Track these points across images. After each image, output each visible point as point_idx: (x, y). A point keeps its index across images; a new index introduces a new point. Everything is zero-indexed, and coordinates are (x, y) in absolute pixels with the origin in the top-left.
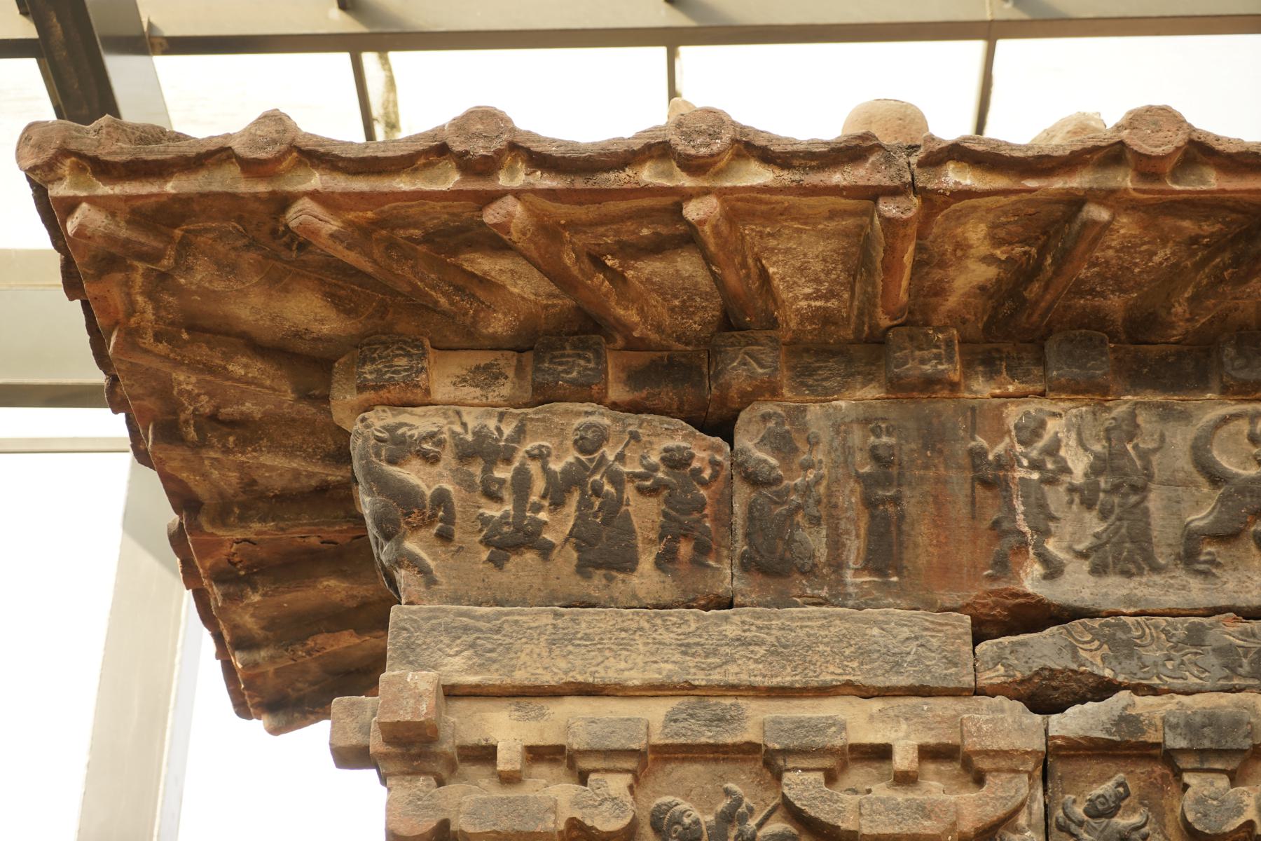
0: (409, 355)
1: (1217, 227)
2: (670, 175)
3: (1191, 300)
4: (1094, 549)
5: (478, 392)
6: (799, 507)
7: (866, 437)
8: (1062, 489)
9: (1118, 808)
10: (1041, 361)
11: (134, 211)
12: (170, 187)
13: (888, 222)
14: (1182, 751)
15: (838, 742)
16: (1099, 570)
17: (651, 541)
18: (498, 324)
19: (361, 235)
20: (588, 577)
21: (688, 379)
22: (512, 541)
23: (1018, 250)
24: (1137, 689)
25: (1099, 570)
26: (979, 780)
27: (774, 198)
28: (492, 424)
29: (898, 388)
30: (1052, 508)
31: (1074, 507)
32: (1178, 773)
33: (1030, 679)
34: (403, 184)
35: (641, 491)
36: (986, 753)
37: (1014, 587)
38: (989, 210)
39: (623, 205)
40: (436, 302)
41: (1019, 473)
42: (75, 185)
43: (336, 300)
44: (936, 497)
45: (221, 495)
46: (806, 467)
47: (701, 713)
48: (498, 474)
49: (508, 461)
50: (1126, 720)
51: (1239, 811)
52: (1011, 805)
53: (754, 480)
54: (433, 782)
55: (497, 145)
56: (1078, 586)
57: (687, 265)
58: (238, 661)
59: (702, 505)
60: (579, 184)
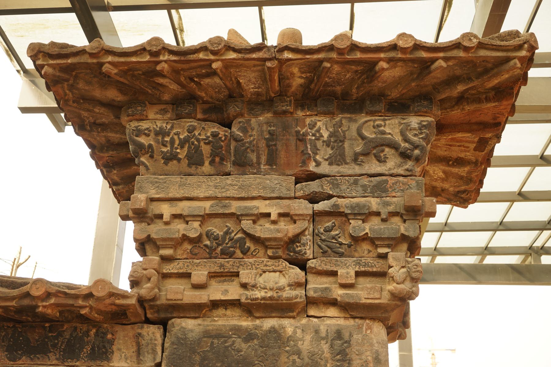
0: (141, 106)
1: (362, 68)
2: (207, 55)
3: (357, 88)
4: (329, 158)
5: (161, 116)
6: (248, 147)
7: (267, 128)
8: (321, 141)
9: (332, 229)
10: (316, 106)
11: (60, 68)
12: (69, 61)
13: (269, 68)
14: (349, 214)
15: (256, 212)
16: (330, 164)
17: (208, 157)
18: (166, 97)
19: (124, 73)
20: (191, 167)
21: (218, 112)
22: (170, 158)
23: (308, 75)
24: (339, 197)
25: (330, 164)
26: (295, 222)
27: (237, 61)
28: (164, 125)
29: (276, 113)
30: (318, 147)
31: (324, 147)
32: (349, 220)
33: (310, 194)
34: (134, 59)
35: (205, 143)
36: (296, 215)
37: (307, 169)
38: (297, 64)
39: (196, 64)
40: (148, 92)
41: (309, 137)
42: (43, 61)
43: (121, 91)
44: (286, 144)
45: (101, 144)
46: (251, 136)
47: (220, 205)
48: (166, 139)
49: (169, 136)
50: (335, 205)
51: (364, 230)
52: (302, 229)
53: (236, 140)
54: (146, 224)
55: (159, 48)
56: (325, 168)
57: (217, 80)
58: (114, 188)
59: (222, 147)
60: (183, 58)
